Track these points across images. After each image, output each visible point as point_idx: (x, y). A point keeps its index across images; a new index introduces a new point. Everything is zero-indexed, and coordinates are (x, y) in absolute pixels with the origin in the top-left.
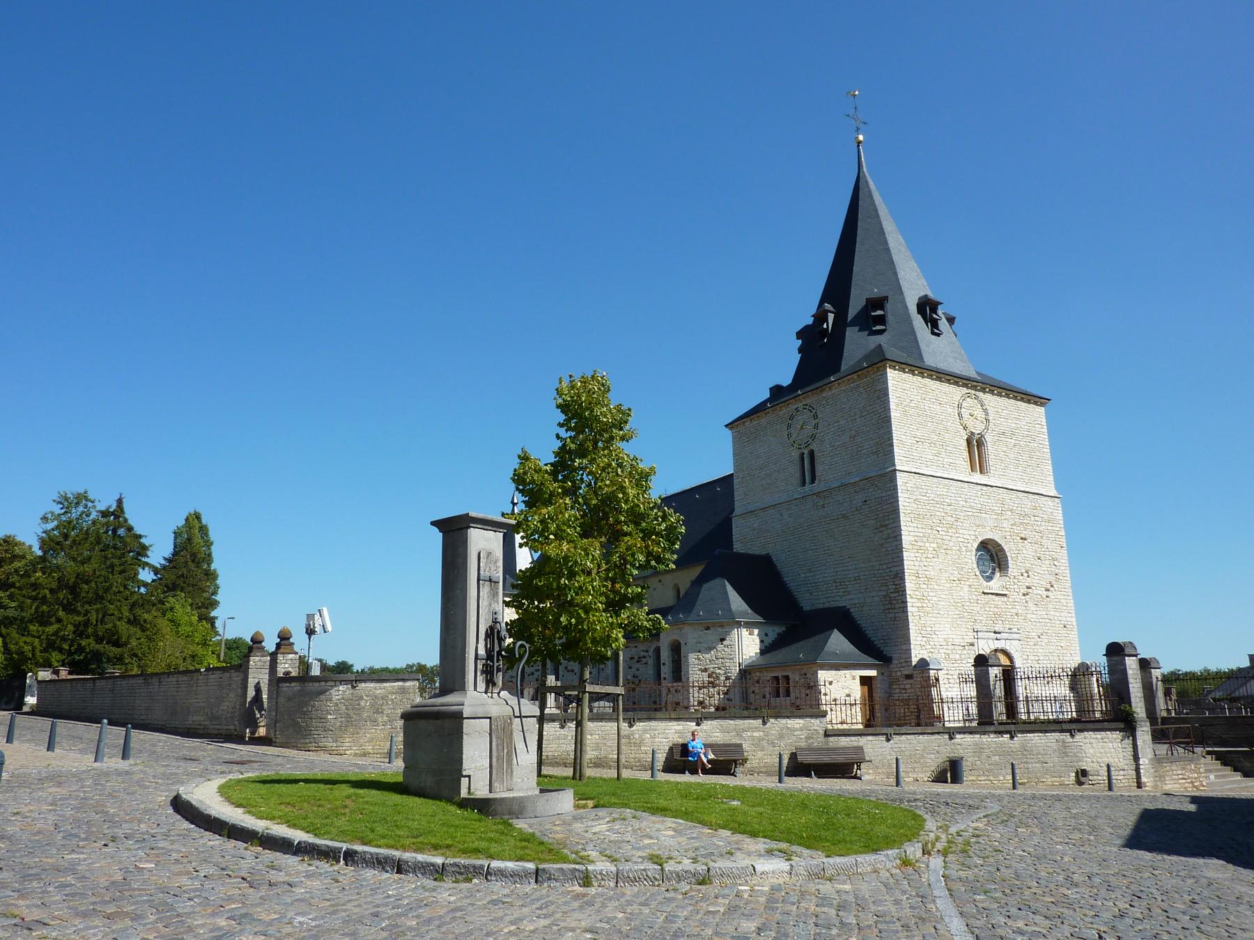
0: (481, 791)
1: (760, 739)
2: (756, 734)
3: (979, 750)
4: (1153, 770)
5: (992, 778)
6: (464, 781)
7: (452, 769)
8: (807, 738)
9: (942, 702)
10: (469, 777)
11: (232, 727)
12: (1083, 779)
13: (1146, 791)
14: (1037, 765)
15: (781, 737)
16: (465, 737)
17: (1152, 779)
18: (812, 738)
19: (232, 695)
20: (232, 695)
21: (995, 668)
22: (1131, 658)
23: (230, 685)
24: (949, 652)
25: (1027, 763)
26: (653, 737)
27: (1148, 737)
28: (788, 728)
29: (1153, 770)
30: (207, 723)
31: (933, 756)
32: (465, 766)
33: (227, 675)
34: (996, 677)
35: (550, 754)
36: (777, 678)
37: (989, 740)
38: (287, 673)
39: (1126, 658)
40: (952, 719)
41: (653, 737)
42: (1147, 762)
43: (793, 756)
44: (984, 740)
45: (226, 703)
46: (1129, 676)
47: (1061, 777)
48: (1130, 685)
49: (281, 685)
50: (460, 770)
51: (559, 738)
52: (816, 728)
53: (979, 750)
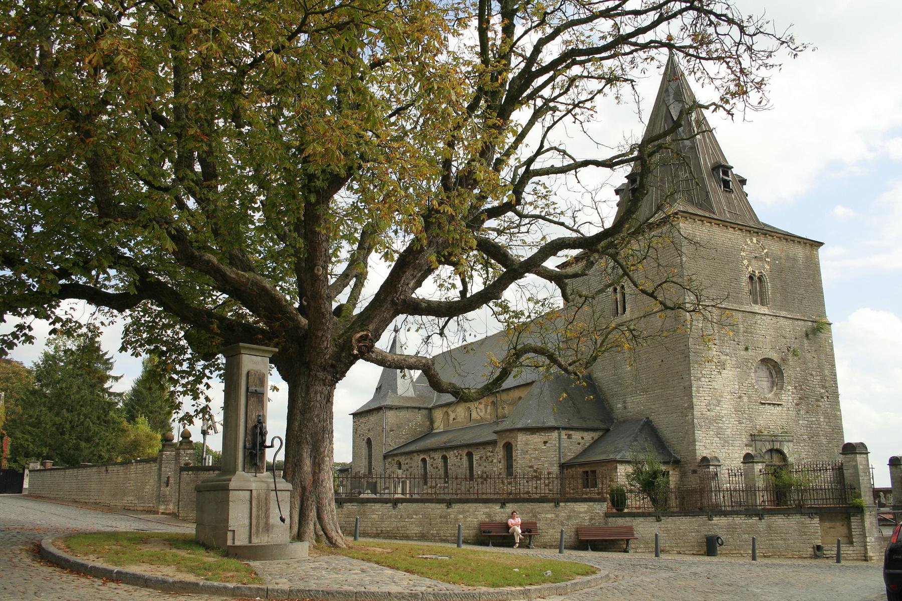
0: (241, 540)
1: (552, 520)
2: (549, 516)
3: (732, 529)
4: (879, 547)
5: (742, 552)
6: (230, 534)
7: (221, 525)
8: (591, 519)
9: (719, 491)
10: (234, 531)
11: (151, 505)
12: (818, 553)
13: (872, 563)
14: (780, 542)
15: (569, 518)
16: (231, 503)
17: (878, 554)
18: (594, 519)
19: (152, 481)
20: (152, 481)
21: (760, 464)
22: (862, 456)
23: (150, 473)
24: (730, 451)
25: (772, 540)
26: (465, 517)
27: (874, 520)
28: (575, 511)
29: (879, 547)
30: (136, 502)
31: (694, 534)
32: (231, 523)
33: (149, 465)
34: (760, 471)
35: (384, 529)
36: (587, 472)
37: (741, 521)
38: (187, 464)
39: (858, 456)
40: (484, 491)
41: (465, 517)
42: (873, 540)
43: (578, 532)
44: (737, 522)
45: (148, 487)
46: (860, 470)
47: (799, 551)
48: (861, 478)
49: (182, 473)
50: (227, 527)
51: (391, 517)
52: (597, 511)
53: (732, 529)
